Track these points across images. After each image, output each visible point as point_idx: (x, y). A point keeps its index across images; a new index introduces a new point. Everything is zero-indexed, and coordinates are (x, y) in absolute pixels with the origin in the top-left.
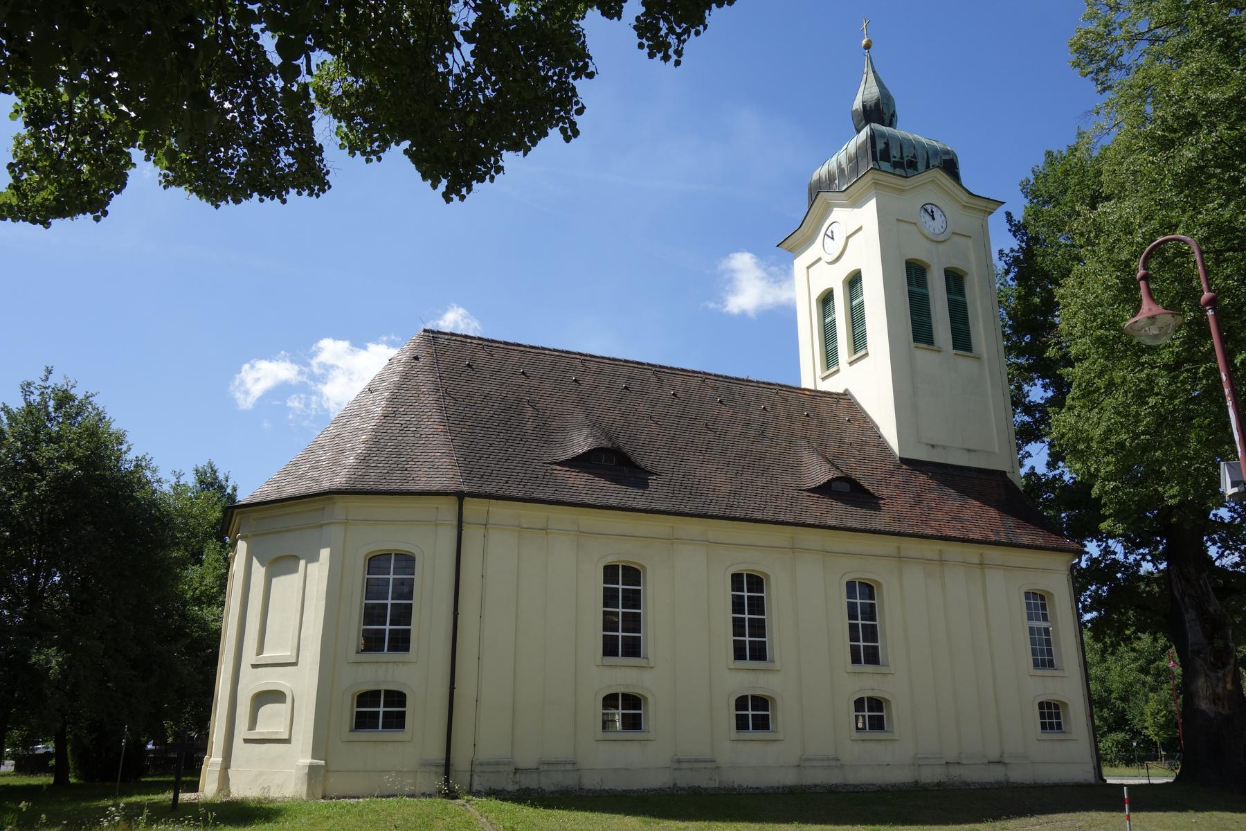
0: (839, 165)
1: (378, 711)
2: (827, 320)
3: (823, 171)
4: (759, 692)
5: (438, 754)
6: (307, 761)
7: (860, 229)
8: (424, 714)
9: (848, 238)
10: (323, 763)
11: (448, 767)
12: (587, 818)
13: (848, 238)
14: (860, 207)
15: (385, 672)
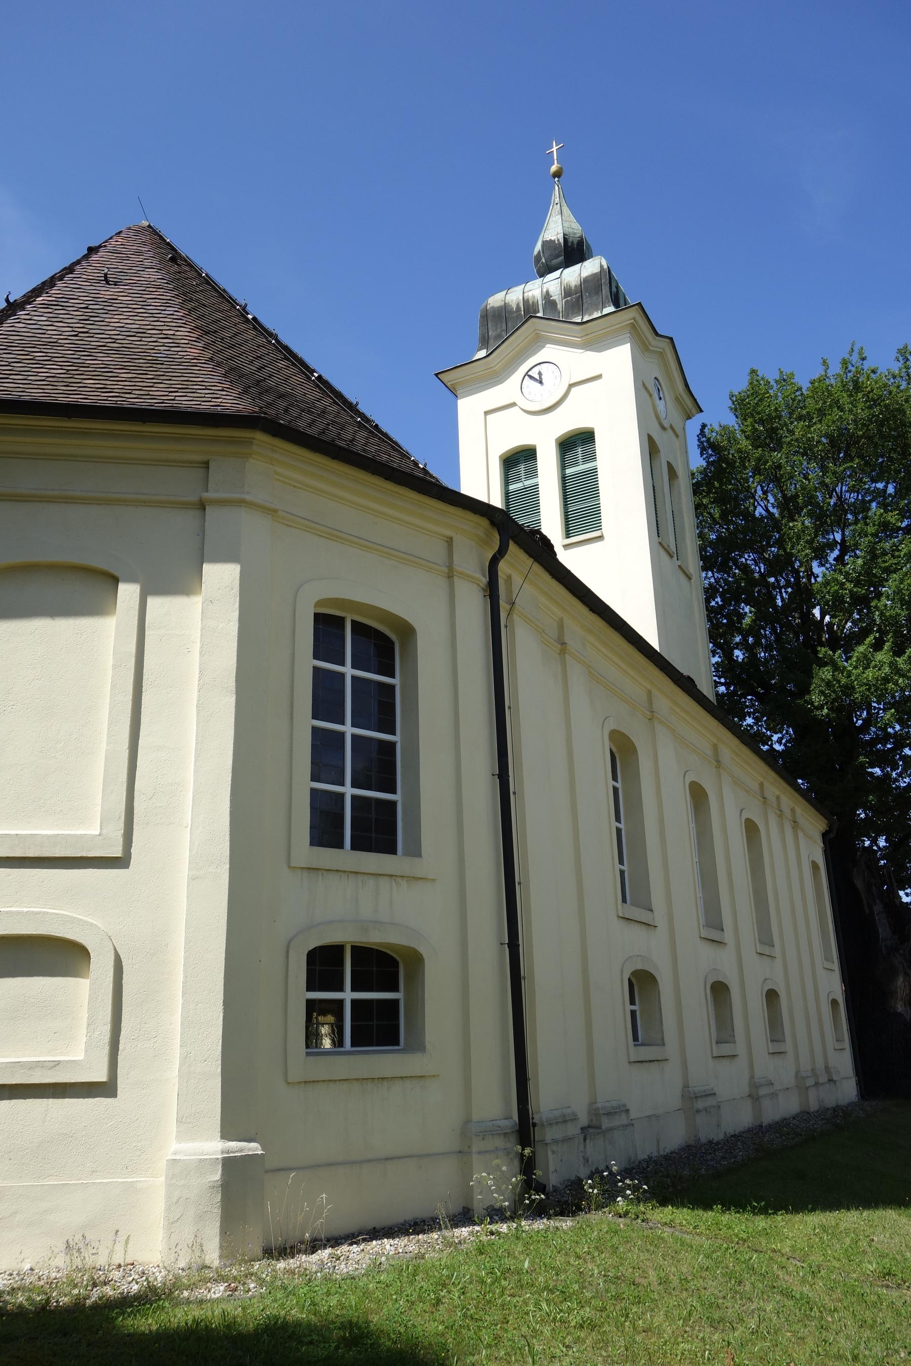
0: (547, 296)
1: (359, 996)
2: (512, 487)
3: (514, 296)
4: (374, 938)
5: (493, 1102)
6: (214, 1147)
7: (599, 377)
8: (455, 1001)
9: (571, 386)
10: (254, 1148)
11: (525, 1130)
12: (834, 1232)
13: (571, 386)
14: (599, 350)
15: (359, 901)
